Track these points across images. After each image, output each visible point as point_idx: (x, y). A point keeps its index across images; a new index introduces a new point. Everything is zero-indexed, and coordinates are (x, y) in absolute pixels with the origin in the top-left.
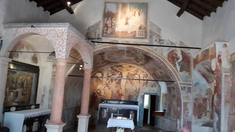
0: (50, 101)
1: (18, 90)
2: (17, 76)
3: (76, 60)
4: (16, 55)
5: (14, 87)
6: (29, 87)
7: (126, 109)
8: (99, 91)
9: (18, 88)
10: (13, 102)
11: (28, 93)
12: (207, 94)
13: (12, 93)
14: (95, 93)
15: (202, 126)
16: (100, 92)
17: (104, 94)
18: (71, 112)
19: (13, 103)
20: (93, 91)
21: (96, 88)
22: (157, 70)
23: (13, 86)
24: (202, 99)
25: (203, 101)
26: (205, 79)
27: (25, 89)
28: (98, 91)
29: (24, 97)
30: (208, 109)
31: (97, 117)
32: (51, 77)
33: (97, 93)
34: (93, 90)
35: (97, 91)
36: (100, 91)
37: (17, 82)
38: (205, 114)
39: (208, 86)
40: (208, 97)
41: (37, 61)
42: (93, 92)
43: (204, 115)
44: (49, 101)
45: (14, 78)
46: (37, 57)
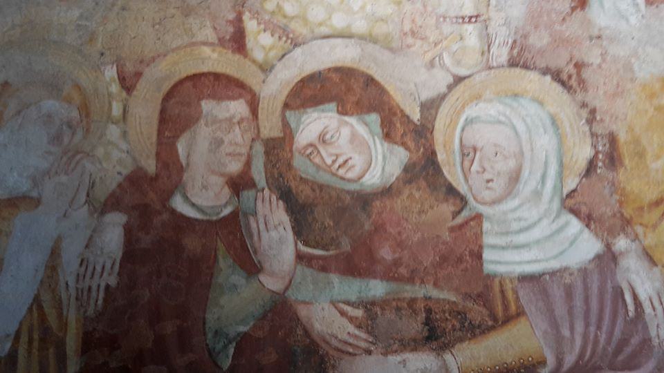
8: (350, 151)
14: (233, 232)
16: (425, 169)
17: (582, 246)
18: (402, 45)
20: (124, 146)
21: (238, 42)
28: (315, 124)
33: (276, 236)
34: (145, 109)
35: (278, 149)
36: (413, 132)
42: (144, 198)
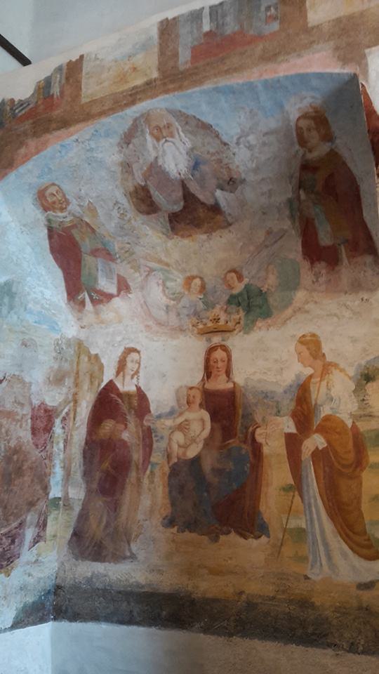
12: (57, 379)
15: (17, 624)
22: (12, 356)
23: (47, 327)
24: (27, 411)
25: (34, 431)
26: (59, 273)
30: (55, 492)
31: (346, 252)
38: (38, 525)
39: (69, 327)
40: (66, 402)
43: (30, 534)
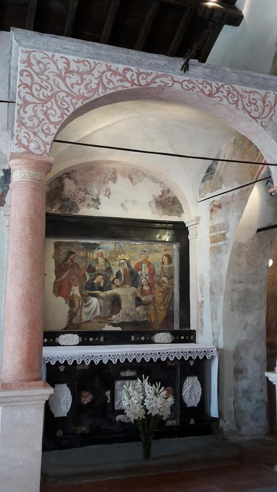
0: (214, 322)
1: (115, 291)
2: (107, 256)
3: (258, 165)
4: (92, 203)
5: (102, 284)
6: (160, 284)
7: (135, 360)
9: (118, 287)
10: (101, 322)
11: (159, 298)
13: (94, 301)
19: (104, 327)
27: (146, 288)
29: (145, 309)
32: (209, 245)
37: (109, 269)
41: (181, 207)
44: (212, 320)
45: (97, 260)
46: (175, 198)
